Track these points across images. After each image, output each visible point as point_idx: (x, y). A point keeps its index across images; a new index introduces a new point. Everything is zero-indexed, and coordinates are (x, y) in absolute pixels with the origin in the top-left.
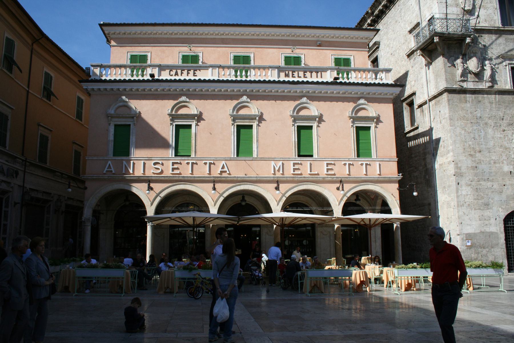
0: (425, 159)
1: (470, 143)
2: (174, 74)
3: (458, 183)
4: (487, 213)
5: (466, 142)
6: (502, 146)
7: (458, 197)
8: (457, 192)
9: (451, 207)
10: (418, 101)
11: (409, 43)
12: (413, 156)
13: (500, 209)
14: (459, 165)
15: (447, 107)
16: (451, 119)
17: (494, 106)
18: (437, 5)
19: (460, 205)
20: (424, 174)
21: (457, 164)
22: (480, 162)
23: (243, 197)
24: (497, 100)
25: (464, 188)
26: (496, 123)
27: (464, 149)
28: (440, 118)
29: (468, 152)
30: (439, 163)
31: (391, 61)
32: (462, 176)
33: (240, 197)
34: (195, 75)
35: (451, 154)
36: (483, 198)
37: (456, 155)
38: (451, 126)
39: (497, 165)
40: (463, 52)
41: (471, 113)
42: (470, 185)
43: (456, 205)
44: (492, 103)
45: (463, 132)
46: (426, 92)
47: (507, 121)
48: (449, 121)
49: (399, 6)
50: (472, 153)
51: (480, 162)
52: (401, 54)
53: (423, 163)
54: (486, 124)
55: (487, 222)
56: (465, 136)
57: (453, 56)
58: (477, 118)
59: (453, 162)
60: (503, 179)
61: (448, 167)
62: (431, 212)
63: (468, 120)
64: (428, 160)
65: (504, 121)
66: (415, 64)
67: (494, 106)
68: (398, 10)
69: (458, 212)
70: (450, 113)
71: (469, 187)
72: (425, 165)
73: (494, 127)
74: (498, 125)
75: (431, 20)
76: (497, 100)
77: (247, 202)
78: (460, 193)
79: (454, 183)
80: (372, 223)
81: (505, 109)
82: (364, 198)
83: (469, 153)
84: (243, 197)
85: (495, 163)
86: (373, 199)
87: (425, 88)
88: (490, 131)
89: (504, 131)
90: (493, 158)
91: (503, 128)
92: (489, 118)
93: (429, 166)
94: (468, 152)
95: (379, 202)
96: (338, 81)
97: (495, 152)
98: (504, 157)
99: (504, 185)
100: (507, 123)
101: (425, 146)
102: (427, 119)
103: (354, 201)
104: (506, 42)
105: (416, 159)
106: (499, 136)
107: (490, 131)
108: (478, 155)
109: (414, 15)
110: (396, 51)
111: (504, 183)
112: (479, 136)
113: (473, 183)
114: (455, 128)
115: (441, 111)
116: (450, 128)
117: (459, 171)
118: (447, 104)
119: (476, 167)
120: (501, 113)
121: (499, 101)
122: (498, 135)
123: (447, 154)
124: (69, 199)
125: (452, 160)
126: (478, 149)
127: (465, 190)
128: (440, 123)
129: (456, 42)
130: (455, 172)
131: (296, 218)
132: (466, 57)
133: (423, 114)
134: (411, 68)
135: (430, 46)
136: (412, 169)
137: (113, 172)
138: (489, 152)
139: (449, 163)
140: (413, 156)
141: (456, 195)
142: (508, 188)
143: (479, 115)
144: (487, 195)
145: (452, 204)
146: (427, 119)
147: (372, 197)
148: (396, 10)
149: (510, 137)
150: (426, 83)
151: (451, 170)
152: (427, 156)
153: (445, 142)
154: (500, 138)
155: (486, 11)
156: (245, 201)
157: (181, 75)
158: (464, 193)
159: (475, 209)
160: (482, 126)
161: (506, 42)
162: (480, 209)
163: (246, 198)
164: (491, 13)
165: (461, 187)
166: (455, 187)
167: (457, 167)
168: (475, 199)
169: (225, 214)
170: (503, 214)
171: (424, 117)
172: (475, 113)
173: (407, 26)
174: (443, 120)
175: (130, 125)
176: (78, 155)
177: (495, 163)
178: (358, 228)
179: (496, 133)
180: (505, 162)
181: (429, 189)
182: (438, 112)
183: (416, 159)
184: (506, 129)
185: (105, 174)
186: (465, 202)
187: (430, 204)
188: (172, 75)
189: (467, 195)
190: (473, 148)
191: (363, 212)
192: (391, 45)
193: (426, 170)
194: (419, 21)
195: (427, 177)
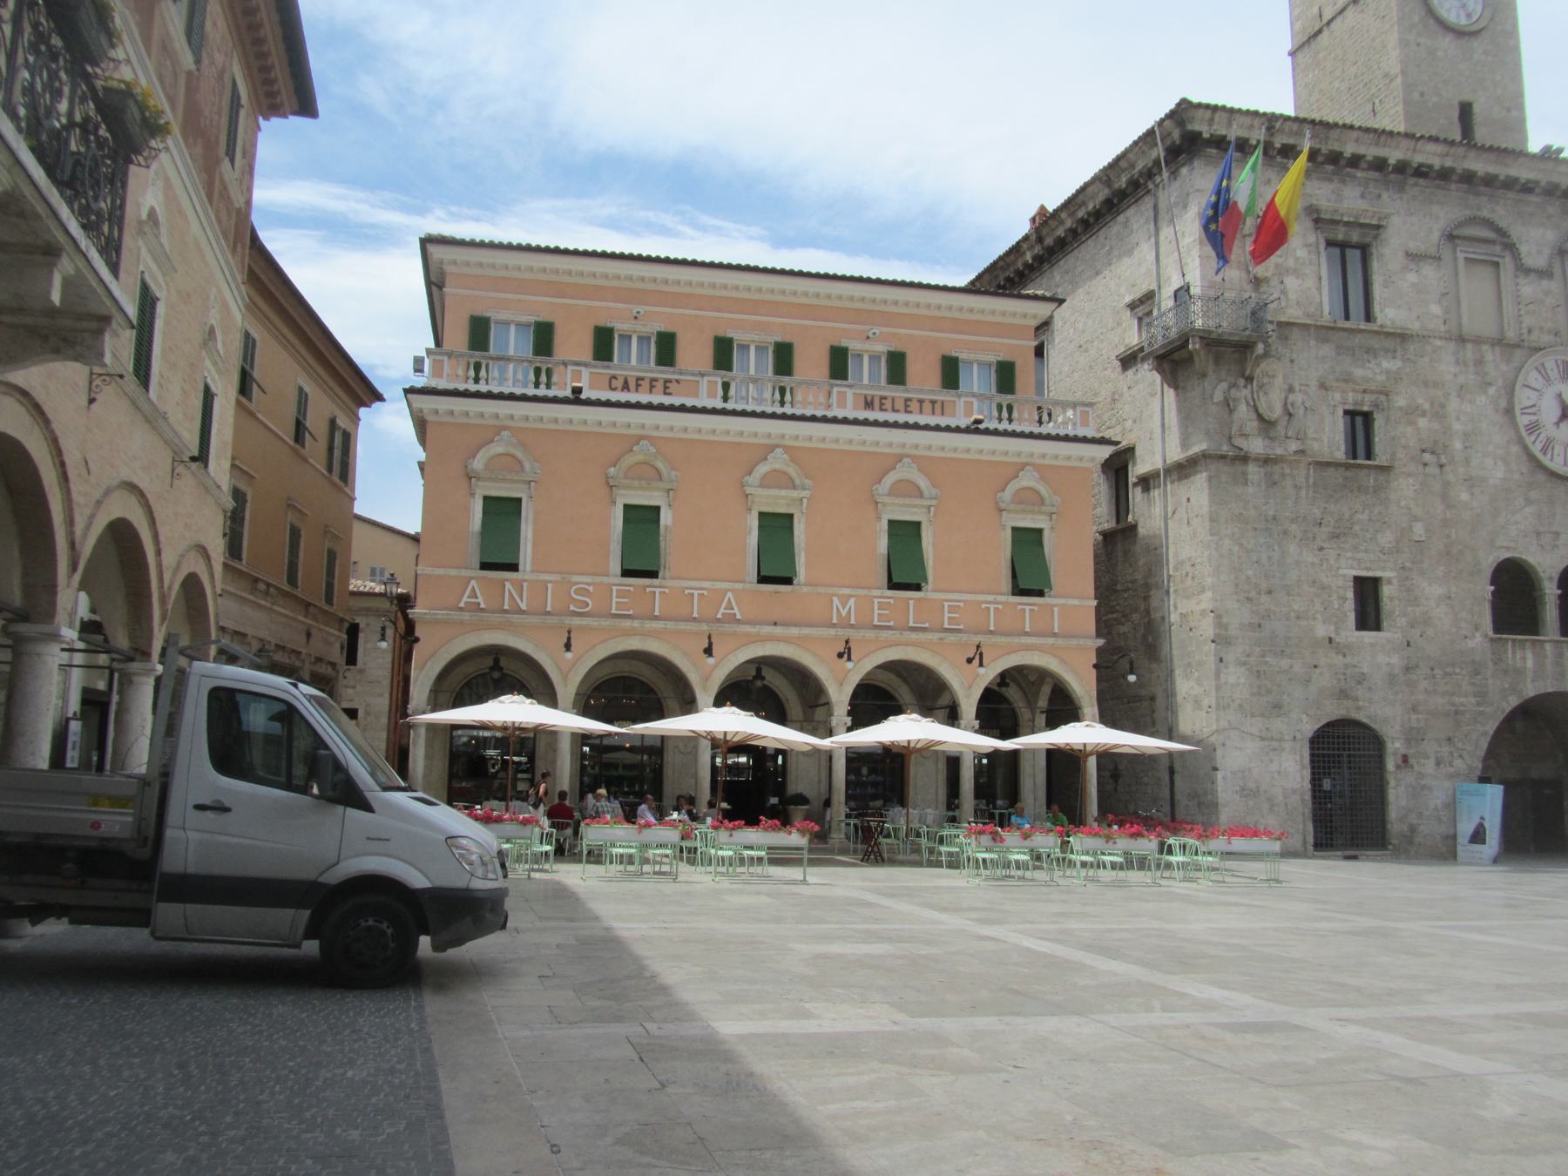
0: (1146, 598)
1: (1250, 573)
2: (620, 387)
3: (1221, 660)
4: (1278, 725)
5: (1240, 570)
6: (1314, 582)
7: (1218, 688)
8: (1217, 675)
9: (1201, 710)
10: (1139, 469)
11: (1125, 331)
12: (1119, 587)
13: (1304, 717)
14: (1225, 620)
15: (1206, 492)
16: (1212, 520)
17: (1303, 492)
18: (1197, 261)
19: (1222, 706)
20: (1142, 631)
21: (1219, 617)
22: (1268, 615)
23: (497, 661)
24: (1311, 481)
25: (1231, 669)
26: (1305, 531)
27: (1237, 585)
28: (1187, 513)
29: (1245, 592)
30: (1179, 611)
31: (1077, 363)
32: (1230, 643)
33: (489, 662)
34: (668, 391)
35: (1209, 594)
36: (1269, 692)
37: (1219, 598)
38: (1212, 535)
39: (1303, 623)
40: (1247, 373)
41: (1255, 507)
42: (1245, 664)
43: (1214, 706)
44: (1301, 488)
45: (1236, 549)
46: (1158, 449)
47: (1328, 529)
48: (1207, 524)
49: (1106, 238)
50: (1253, 594)
51: (1268, 615)
52: (1104, 352)
53: (1142, 608)
54: (1285, 532)
55: (1275, 744)
56: (1239, 557)
57: (1226, 381)
58: (1267, 520)
59: (1212, 612)
60: (1313, 653)
61: (1200, 621)
62: (1155, 715)
63: (1247, 524)
64: (1154, 603)
65: (1323, 529)
66: (1137, 383)
67: (1303, 492)
68: (1103, 247)
69: (1217, 720)
70: (1211, 507)
71: (1243, 669)
72: (1148, 612)
73: (1301, 540)
74: (1310, 535)
75: (1182, 293)
76: (1311, 481)
77: (765, 682)
78: (1223, 680)
79: (1212, 658)
80: (912, 745)
81: (1327, 502)
82: (1014, 680)
83: (1246, 595)
84: (497, 661)
85: (1298, 617)
86: (1033, 683)
87: (1158, 442)
88: (1292, 548)
89: (1321, 549)
90: (1296, 607)
91: (1319, 543)
92: (1293, 521)
93: (1156, 616)
94: (1245, 592)
95: (1046, 690)
96: (982, 426)
97: (1299, 595)
98: (1318, 606)
99: (1315, 667)
100: (1329, 532)
101: (1150, 570)
102: (1158, 510)
103: (997, 688)
104: (1338, 354)
105: (1126, 596)
106: (1310, 560)
107: (1292, 548)
108: (1264, 598)
109: (1143, 270)
110: (1092, 342)
111: (1315, 662)
112: (1270, 558)
113: (1252, 659)
114: (1221, 539)
115: (1192, 500)
116: (1210, 538)
117: (1223, 632)
118: (1205, 485)
119: (1260, 626)
120: (1317, 511)
121: (1314, 483)
122: (1309, 557)
123: (1199, 594)
124: (319, 660)
125: (1211, 607)
126: (1264, 585)
127: (1235, 676)
128: (1188, 523)
129: (1233, 349)
130: (1215, 635)
131: (610, 735)
132: (1252, 384)
133: (1149, 500)
134: (1125, 389)
135: (1176, 354)
136: (1115, 616)
137: (482, 606)
138: (1288, 594)
139: (1203, 613)
140: (1119, 587)
141: (1214, 683)
142: (1321, 674)
143: (1271, 513)
144: (1279, 686)
145: (1206, 702)
146: (1158, 510)
147: (1032, 678)
148: (1099, 247)
149: (1332, 562)
150: (1159, 430)
151: (1207, 628)
152: (1152, 593)
153: (1198, 567)
154: (1313, 564)
155: (1300, 281)
156: (501, 669)
157: (637, 391)
158: (1232, 680)
159: (1253, 715)
160: (1275, 537)
161: (1338, 354)
162: (1262, 715)
163: (503, 662)
164: (1310, 289)
165: (1226, 667)
166: (1213, 666)
167: (1219, 624)
168: (1253, 694)
169: (451, 704)
170: (1309, 727)
171: (1150, 506)
172: (1264, 508)
173: (1123, 290)
174: (1195, 519)
175: (519, 500)
176: (332, 555)
177: (1298, 617)
178: (625, 784)
179: (1304, 553)
180: (1319, 616)
181: (1154, 666)
182: (1185, 499)
183: (1126, 596)
184: (1325, 545)
185: (461, 609)
186: (1233, 701)
187: (1153, 699)
188: (615, 389)
189: (1238, 684)
190: (1255, 583)
191: (661, 714)
192: (1080, 326)
193: (1149, 622)
194: (1154, 287)
195: (1150, 639)
